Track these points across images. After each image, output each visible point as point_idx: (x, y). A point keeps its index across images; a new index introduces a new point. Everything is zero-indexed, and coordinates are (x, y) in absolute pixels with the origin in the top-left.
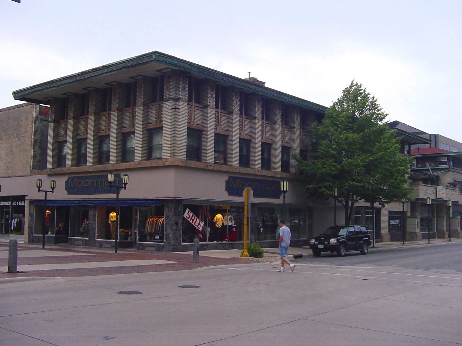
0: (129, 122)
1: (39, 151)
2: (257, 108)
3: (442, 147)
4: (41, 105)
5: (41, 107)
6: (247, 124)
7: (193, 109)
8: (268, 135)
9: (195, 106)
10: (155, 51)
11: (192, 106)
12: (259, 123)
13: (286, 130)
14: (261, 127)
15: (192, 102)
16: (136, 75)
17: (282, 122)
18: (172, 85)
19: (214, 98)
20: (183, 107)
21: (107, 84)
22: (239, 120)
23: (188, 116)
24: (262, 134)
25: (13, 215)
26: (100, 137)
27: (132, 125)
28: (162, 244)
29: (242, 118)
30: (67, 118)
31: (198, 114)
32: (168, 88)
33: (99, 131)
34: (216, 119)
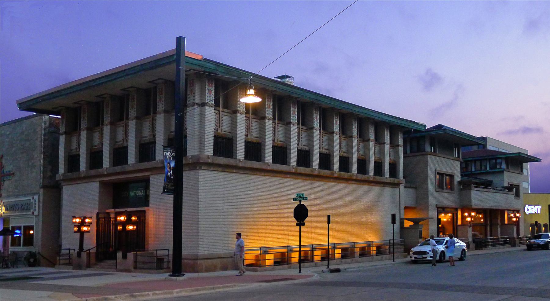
1: (49, 168)
3: (490, 147)
4: (50, 116)
5: (51, 118)
7: (221, 115)
8: (281, 137)
9: (302, 128)
10: (440, 124)
11: (249, 118)
13: (254, 121)
14: (297, 133)
15: (219, 107)
16: (157, 78)
17: (320, 126)
19: (271, 109)
20: (210, 112)
21: (124, 90)
22: (272, 126)
23: (215, 123)
24: (298, 141)
25: (309, 251)
29: (275, 123)
34: (246, 125)
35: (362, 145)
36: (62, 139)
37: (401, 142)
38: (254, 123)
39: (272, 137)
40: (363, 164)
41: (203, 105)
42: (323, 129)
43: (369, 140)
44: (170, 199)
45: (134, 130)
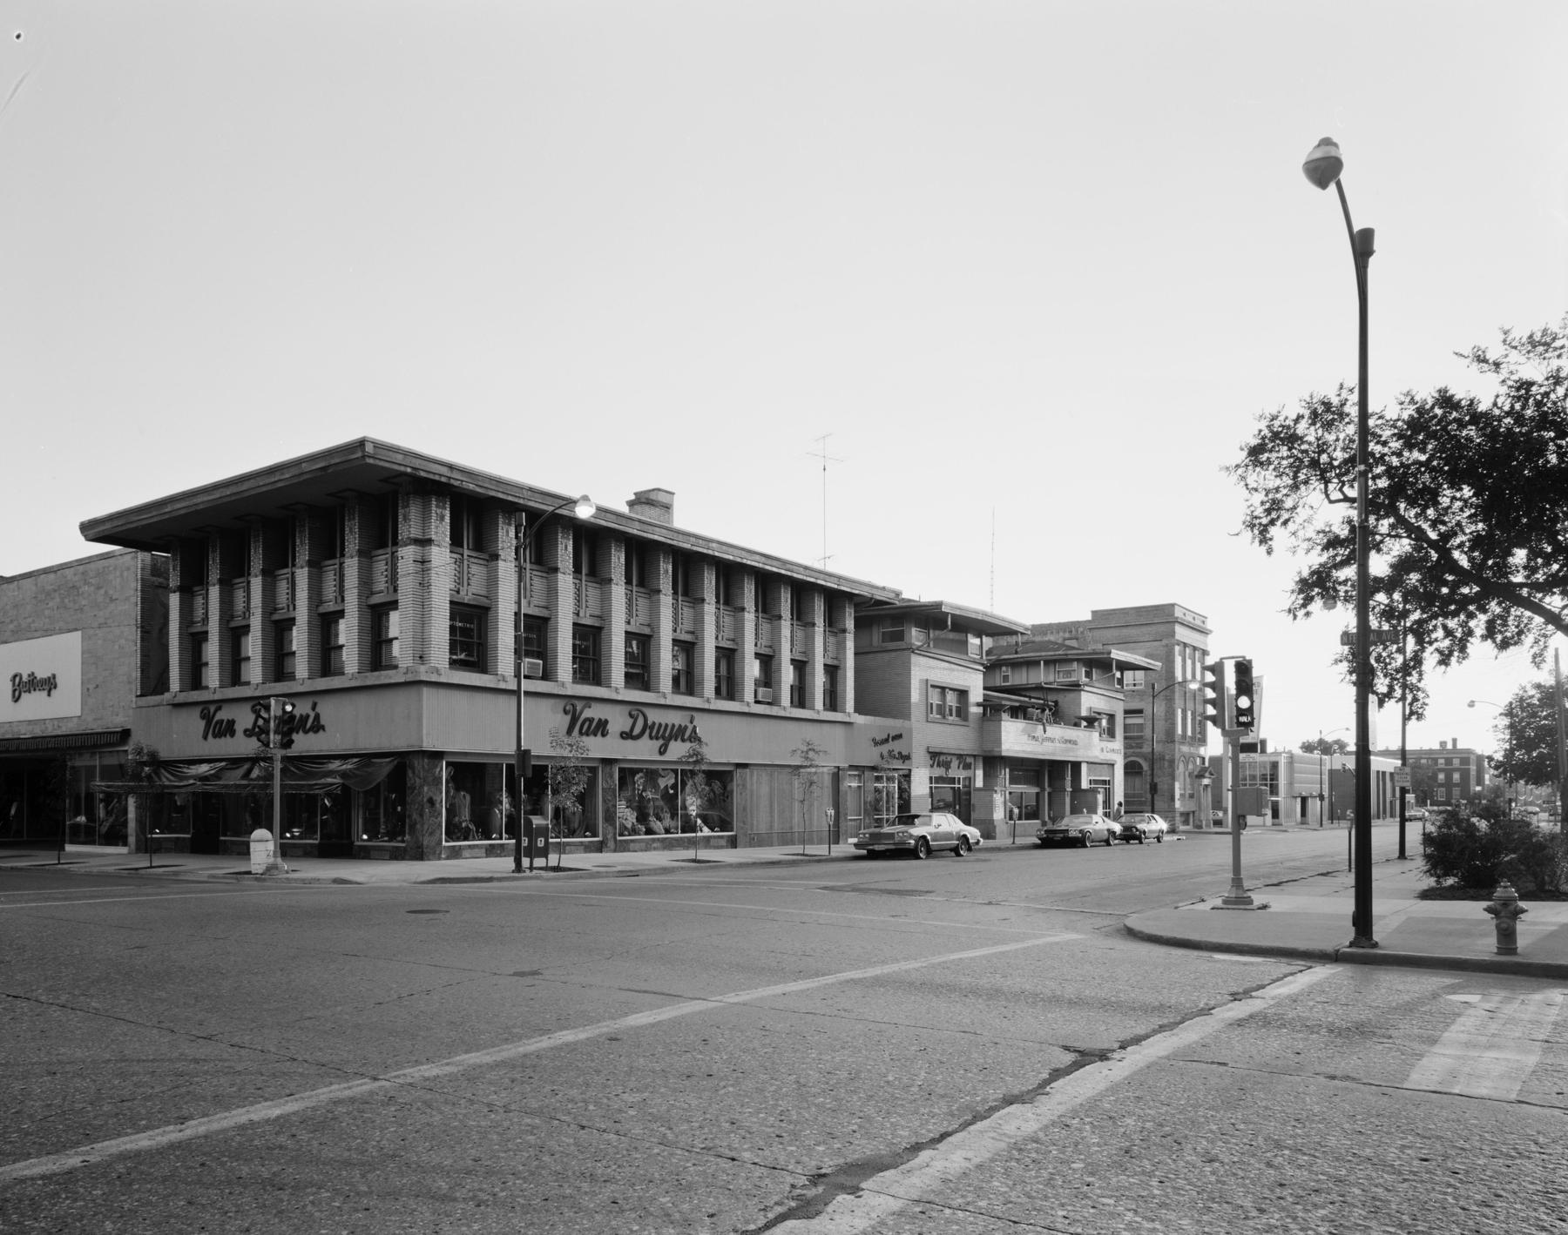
0: (387, 582)
2: (614, 559)
6: (592, 593)
11: (462, 555)
12: (618, 591)
18: (414, 511)
20: (441, 555)
26: (373, 607)
27: (391, 589)
28: (404, 845)
30: (343, 555)
31: (477, 571)
32: (406, 518)
33: (321, 602)
35: (832, 639)
36: (174, 600)
37: (850, 624)
38: (727, 619)
39: (671, 624)
40: (535, 634)
41: (425, 542)
42: (798, 619)
43: (844, 631)
44: (593, 705)
45: (305, 587)
